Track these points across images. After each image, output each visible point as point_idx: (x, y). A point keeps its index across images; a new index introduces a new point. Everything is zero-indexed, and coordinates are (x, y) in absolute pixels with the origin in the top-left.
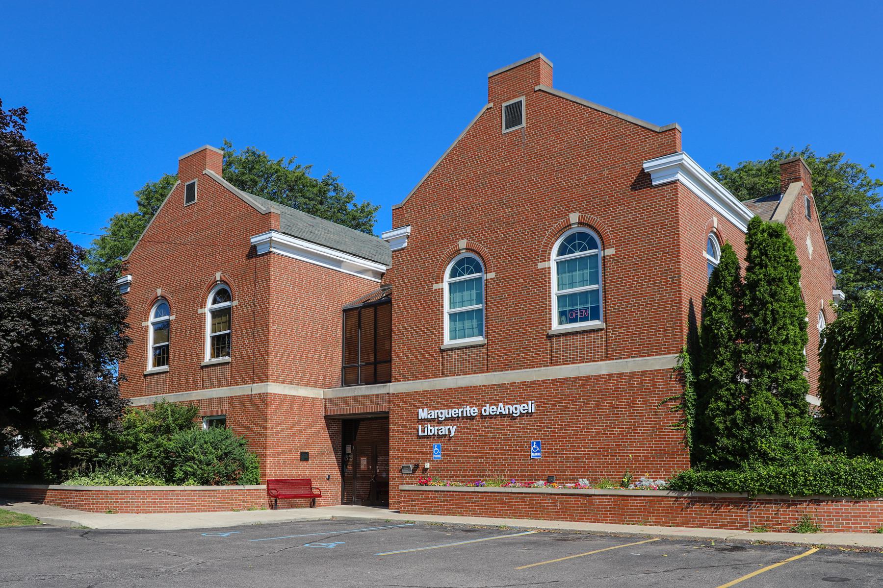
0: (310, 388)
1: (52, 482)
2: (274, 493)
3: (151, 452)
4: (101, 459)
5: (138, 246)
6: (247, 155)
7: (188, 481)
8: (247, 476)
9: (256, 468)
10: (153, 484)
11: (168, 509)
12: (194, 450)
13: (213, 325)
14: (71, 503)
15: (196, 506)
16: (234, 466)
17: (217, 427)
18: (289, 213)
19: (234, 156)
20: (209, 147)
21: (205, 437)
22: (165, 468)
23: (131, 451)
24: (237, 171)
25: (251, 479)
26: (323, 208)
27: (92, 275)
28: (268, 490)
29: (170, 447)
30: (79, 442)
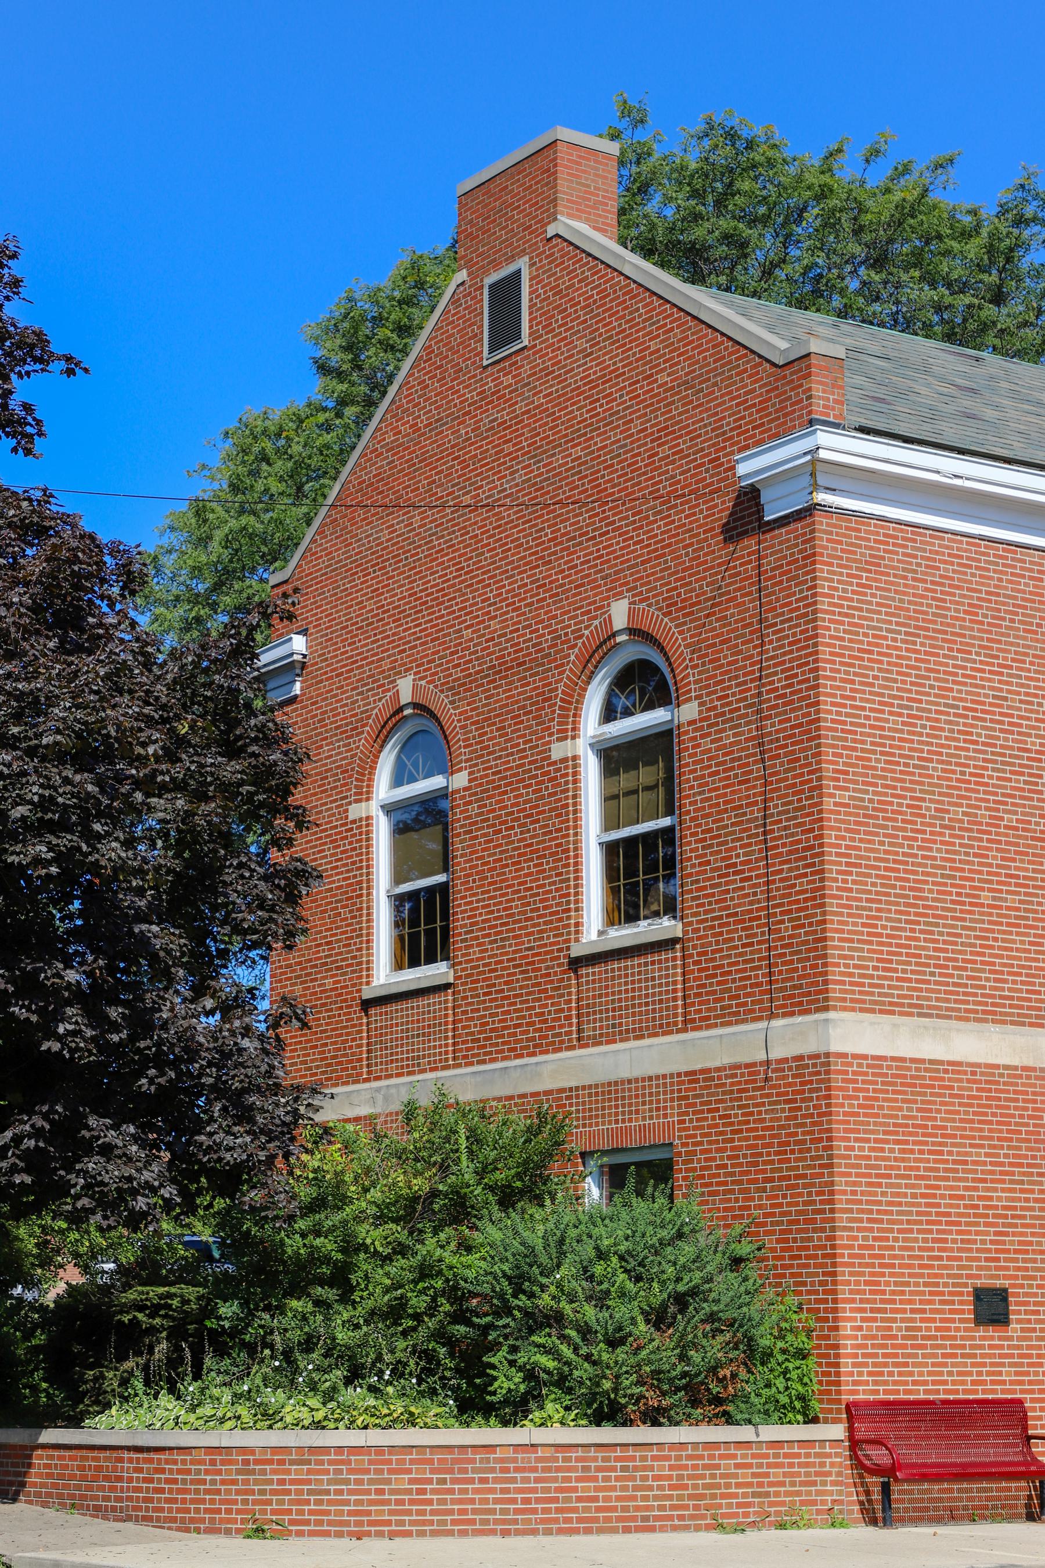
0: (998, 1028)
1: (51, 1417)
2: (879, 1456)
3: (402, 1297)
4: (227, 1324)
5: (322, 525)
6: (707, 143)
7: (541, 1408)
8: (768, 1386)
9: (802, 1354)
10: (411, 1421)
11: (473, 1522)
12: (559, 1286)
13: (609, 799)
14: (119, 1499)
15: (575, 1510)
16: (715, 1348)
17: (640, 1193)
18: (875, 349)
19: (656, 156)
20: (565, 133)
21: (595, 1232)
22: (451, 1355)
23: (330, 1294)
24: (669, 212)
25: (784, 1399)
26: (1003, 316)
27: (170, 641)
28: (854, 1443)
29: (471, 1274)
30: (141, 1263)
